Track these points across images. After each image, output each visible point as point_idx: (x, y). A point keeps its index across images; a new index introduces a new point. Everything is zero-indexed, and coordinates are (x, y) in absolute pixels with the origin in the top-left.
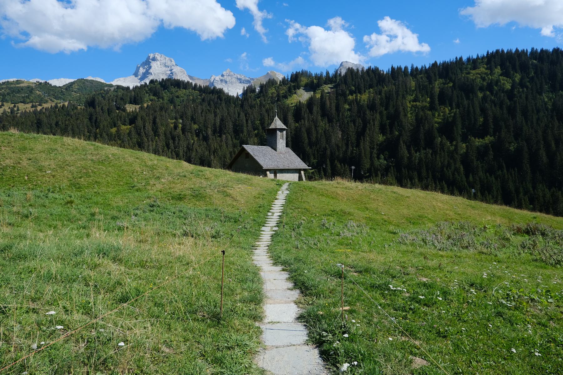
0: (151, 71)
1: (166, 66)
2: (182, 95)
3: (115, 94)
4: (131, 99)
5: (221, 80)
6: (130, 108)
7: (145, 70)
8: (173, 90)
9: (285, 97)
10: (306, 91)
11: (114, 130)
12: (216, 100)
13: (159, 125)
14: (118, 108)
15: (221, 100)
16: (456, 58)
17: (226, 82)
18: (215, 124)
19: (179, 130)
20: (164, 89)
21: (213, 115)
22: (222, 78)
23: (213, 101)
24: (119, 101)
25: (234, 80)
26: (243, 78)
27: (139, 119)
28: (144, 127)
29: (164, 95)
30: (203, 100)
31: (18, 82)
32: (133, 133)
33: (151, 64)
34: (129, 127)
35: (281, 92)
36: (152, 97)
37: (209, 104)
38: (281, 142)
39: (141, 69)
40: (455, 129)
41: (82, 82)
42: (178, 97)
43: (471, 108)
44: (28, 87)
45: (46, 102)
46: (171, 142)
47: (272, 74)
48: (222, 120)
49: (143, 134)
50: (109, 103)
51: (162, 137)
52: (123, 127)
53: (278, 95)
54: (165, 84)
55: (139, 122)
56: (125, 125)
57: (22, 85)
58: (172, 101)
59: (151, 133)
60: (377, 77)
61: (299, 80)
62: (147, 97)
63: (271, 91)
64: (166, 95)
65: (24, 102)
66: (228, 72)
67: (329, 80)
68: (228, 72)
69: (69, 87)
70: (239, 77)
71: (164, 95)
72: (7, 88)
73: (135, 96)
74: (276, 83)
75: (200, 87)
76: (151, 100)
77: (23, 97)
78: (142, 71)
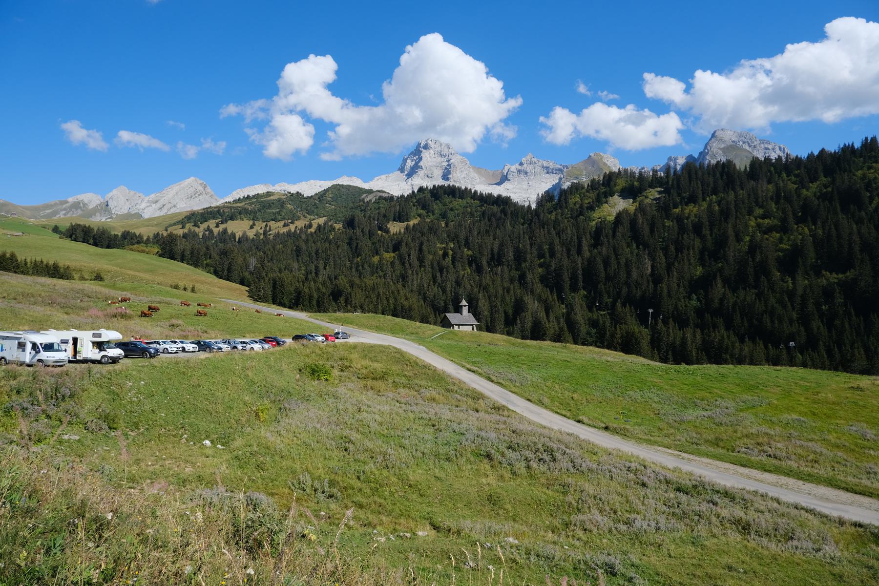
0: (421, 164)
1: (441, 155)
2: (457, 207)
3: (376, 206)
4: (395, 215)
5: (519, 171)
6: (395, 228)
7: (413, 163)
8: (447, 199)
9: (591, 208)
10: (623, 198)
11: (376, 259)
12: (499, 214)
13: (426, 253)
14: (380, 229)
15: (505, 215)
16: (866, 139)
17: (526, 173)
18: (492, 250)
19: (449, 259)
20: (436, 199)
21: (491, 237)
22: (519, 167)
23: (495, 216)
24: (381, 218)
25: (538, 169)
26: (551, 165)
27: (404, 245)
28: (409, 256)
29: (435, 207)
30: (484, 213)
31: (269, 194)
32: (397, 263)
33: (422, 155)
34: (393, 255)
35: (587, 202)
36: (421, 211)
37: (490, 220)
38: (465, 310)
39: (408, 161)
40: (800, 260)
41: (337, 188)
42: (452, 210)
43: (833, 230)
44: (279, 200)
45: (299, 218)
46: (438, 274)
47: (595, 158)
48: (502, 245)
49: (407, 266)
50: (370, 224)
51: (429, 269)
52: (387, 255)
53: (581, 207)
54: (437, 193)
55: (404, 249)
56: (387, 252)
57: (272, 198)
58: (444, 216)
59: (416, 263)
60: (725, 177)
61: (612, 183)
62: (414, 211)
63: (573, 200)
64: (437, 207)
65: (275, 220)
66: (529, 157)
67: (656, 181)
68: (529, 157)
69: (321, 196)
70: (545, 164)
71: (435, 207)
72: (257, 202)
73: (398, 208)
74: (583, 188)
75: (481, 194)
76: (420, 216)
77: (274, 214)
78: (409, 164)
